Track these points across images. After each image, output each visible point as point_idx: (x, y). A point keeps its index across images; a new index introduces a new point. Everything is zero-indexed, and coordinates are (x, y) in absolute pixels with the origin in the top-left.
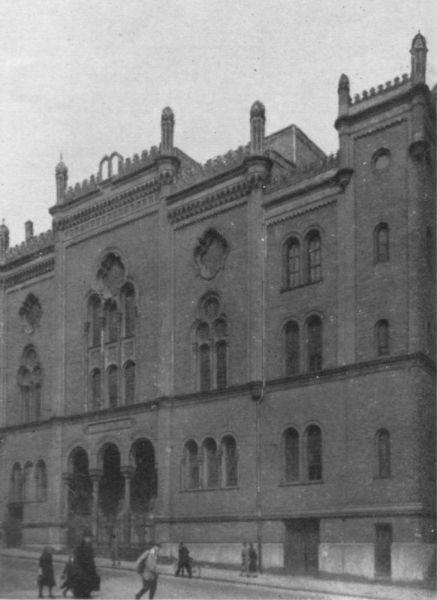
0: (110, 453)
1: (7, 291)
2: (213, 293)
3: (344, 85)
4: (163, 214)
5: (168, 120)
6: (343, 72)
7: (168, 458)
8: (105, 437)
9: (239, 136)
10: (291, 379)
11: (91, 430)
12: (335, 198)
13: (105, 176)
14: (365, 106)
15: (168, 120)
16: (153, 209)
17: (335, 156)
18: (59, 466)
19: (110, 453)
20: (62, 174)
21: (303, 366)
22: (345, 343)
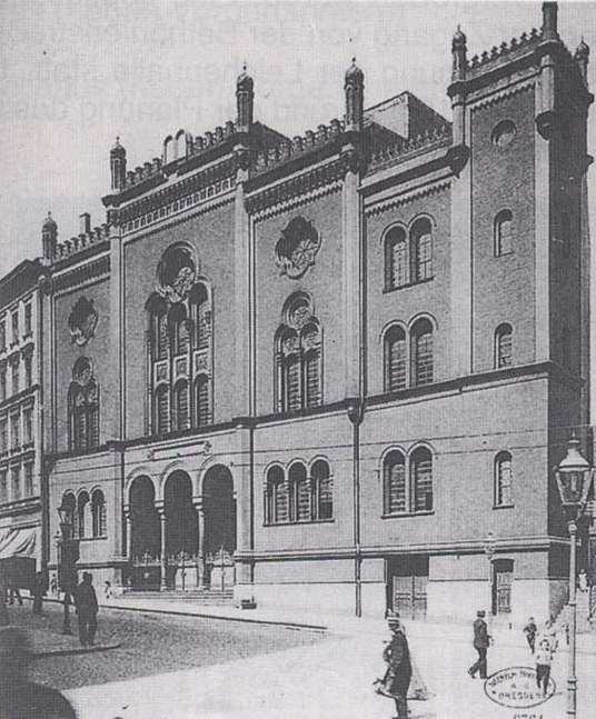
0: (179, 481)
1: (56, 294)
2: (304, 294)
3: (118, 154)
4: (239, 203)
5: (245, 88)
6: (371, 690)
7: (249, 491)
8: (174, 464)
9: (333, 106)
10: (392, 395)
11: (157, 455)
12: (447, 181)
13: (170, 159)
14: (482, 72)
15: (245, 88)
16: (230, 196)
17: (409, 716)
18: (115, 499)
19: (179, 481)
20: (459, 45)
21: (414, 279)
22: (456, 350)
